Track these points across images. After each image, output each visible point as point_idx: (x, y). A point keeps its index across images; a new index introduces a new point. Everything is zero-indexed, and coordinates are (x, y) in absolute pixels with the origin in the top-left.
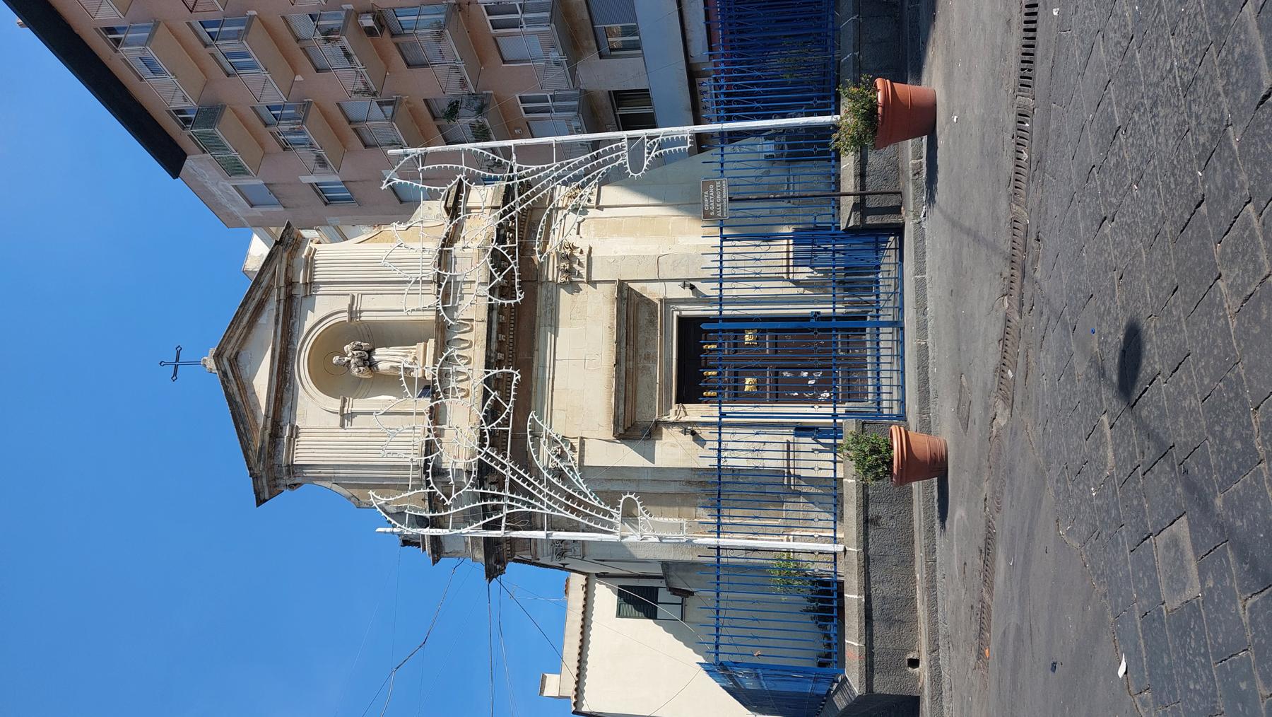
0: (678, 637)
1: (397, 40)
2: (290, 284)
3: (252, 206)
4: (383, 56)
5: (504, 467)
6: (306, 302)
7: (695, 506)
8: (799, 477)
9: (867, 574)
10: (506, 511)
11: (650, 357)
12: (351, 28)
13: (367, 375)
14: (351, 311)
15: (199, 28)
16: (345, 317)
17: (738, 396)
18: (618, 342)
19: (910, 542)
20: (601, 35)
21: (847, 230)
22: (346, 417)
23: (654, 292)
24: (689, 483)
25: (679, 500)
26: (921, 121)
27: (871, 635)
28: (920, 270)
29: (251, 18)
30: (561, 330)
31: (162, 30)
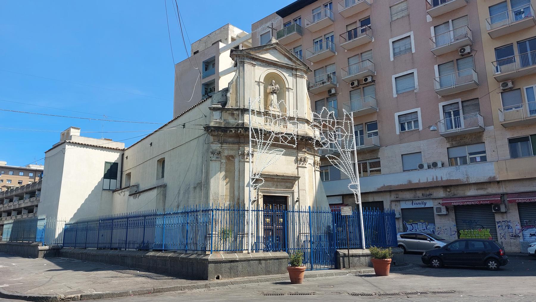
0: (96, 187)
1: (326, 99)
2: (296, 70)
3: (261, 35)
4: (320, 94)
5: (270, 141)
6: (291, 74)
7: (230, 201)
8: (242, 238)
9: (245, 261)
10: (258, 141)
11: (277, 187)
12: (332, 85)
13: (268, 91)
14: (289, 88)
15: (331, 34)
16: (287, 86)
17: (265, 216)
18: (283, 176)
19: (254, 275)
20: (326, 168)
21: (337, 253)
22: (259, 83)
23: (295, 188)
24: (239, 199)
25: (232, 195)
26: (380, 273)
27: (226, 263)
28: (336, 274)
29: (335, 53)
30: (284, 156)
31: (332, 23)
